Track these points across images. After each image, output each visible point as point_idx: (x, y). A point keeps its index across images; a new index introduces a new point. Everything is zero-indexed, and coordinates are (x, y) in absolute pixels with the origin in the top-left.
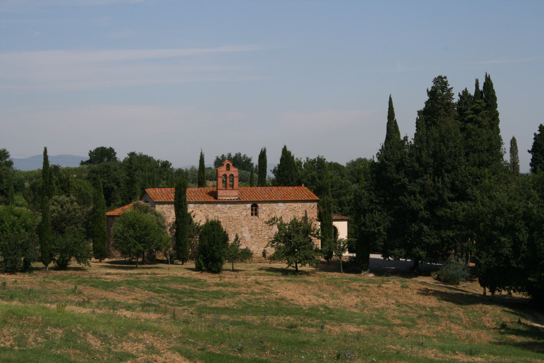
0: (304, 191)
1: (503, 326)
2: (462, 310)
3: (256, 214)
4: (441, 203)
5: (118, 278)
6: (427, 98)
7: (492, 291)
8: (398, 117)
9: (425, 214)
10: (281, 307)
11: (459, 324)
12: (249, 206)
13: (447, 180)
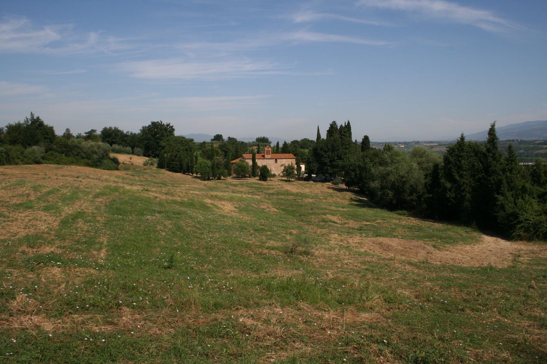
0: (291, 155)
1: (351, 199)
4: (334, 160)
5: (237, 183)
7: (349, 187)
8: (320, 132)
9: (329, 164)
10: (288, 193)
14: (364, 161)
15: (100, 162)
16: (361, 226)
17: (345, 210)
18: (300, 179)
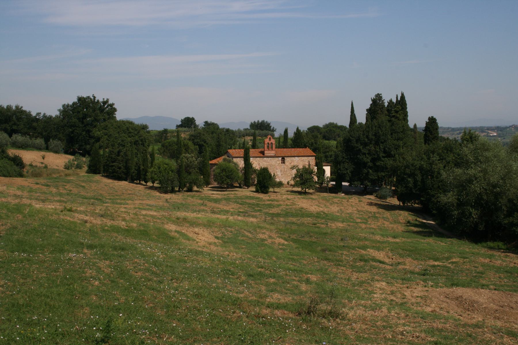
0: (308, 151)
1: (409, 222)
2: (389, 213)
3: (284, 163)
4: (379, 159)
5: (219, 197)
6: (371, 102)
7: (404, 203)
8: (355, 112)
9: (370, 164)
10: (302, 213)
11: (388, 221)
12: (280, 158)
13: (382, 147)
14: (429, 159)
16: (424, 268)
18: (322, 189)
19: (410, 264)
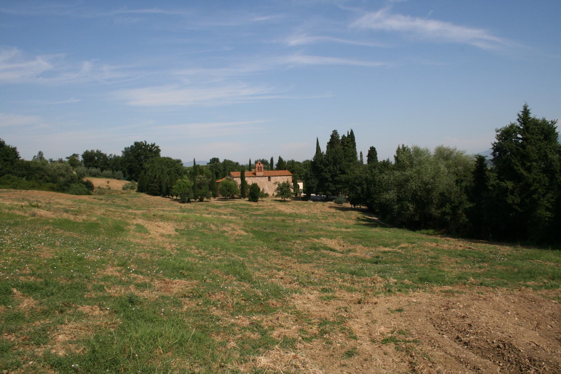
1: (358, 218)
4: (336, 175)
5: (221, 204)
7: (354, 206)
8: (320, 145)
9: (330, 179)
10: (279, 214)
14: (372, 172)
15: (68, 186)
16: (375, 255)
17: (349, 230)
18: (297, 198)
19: (361, 251)
